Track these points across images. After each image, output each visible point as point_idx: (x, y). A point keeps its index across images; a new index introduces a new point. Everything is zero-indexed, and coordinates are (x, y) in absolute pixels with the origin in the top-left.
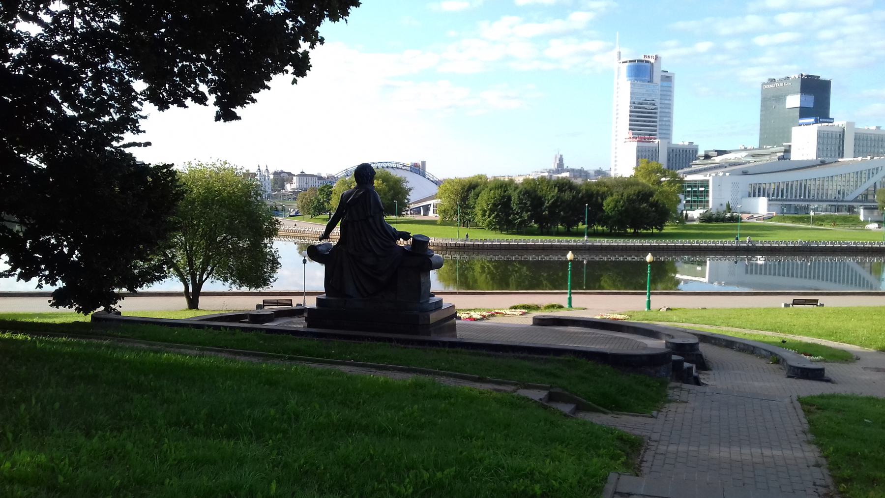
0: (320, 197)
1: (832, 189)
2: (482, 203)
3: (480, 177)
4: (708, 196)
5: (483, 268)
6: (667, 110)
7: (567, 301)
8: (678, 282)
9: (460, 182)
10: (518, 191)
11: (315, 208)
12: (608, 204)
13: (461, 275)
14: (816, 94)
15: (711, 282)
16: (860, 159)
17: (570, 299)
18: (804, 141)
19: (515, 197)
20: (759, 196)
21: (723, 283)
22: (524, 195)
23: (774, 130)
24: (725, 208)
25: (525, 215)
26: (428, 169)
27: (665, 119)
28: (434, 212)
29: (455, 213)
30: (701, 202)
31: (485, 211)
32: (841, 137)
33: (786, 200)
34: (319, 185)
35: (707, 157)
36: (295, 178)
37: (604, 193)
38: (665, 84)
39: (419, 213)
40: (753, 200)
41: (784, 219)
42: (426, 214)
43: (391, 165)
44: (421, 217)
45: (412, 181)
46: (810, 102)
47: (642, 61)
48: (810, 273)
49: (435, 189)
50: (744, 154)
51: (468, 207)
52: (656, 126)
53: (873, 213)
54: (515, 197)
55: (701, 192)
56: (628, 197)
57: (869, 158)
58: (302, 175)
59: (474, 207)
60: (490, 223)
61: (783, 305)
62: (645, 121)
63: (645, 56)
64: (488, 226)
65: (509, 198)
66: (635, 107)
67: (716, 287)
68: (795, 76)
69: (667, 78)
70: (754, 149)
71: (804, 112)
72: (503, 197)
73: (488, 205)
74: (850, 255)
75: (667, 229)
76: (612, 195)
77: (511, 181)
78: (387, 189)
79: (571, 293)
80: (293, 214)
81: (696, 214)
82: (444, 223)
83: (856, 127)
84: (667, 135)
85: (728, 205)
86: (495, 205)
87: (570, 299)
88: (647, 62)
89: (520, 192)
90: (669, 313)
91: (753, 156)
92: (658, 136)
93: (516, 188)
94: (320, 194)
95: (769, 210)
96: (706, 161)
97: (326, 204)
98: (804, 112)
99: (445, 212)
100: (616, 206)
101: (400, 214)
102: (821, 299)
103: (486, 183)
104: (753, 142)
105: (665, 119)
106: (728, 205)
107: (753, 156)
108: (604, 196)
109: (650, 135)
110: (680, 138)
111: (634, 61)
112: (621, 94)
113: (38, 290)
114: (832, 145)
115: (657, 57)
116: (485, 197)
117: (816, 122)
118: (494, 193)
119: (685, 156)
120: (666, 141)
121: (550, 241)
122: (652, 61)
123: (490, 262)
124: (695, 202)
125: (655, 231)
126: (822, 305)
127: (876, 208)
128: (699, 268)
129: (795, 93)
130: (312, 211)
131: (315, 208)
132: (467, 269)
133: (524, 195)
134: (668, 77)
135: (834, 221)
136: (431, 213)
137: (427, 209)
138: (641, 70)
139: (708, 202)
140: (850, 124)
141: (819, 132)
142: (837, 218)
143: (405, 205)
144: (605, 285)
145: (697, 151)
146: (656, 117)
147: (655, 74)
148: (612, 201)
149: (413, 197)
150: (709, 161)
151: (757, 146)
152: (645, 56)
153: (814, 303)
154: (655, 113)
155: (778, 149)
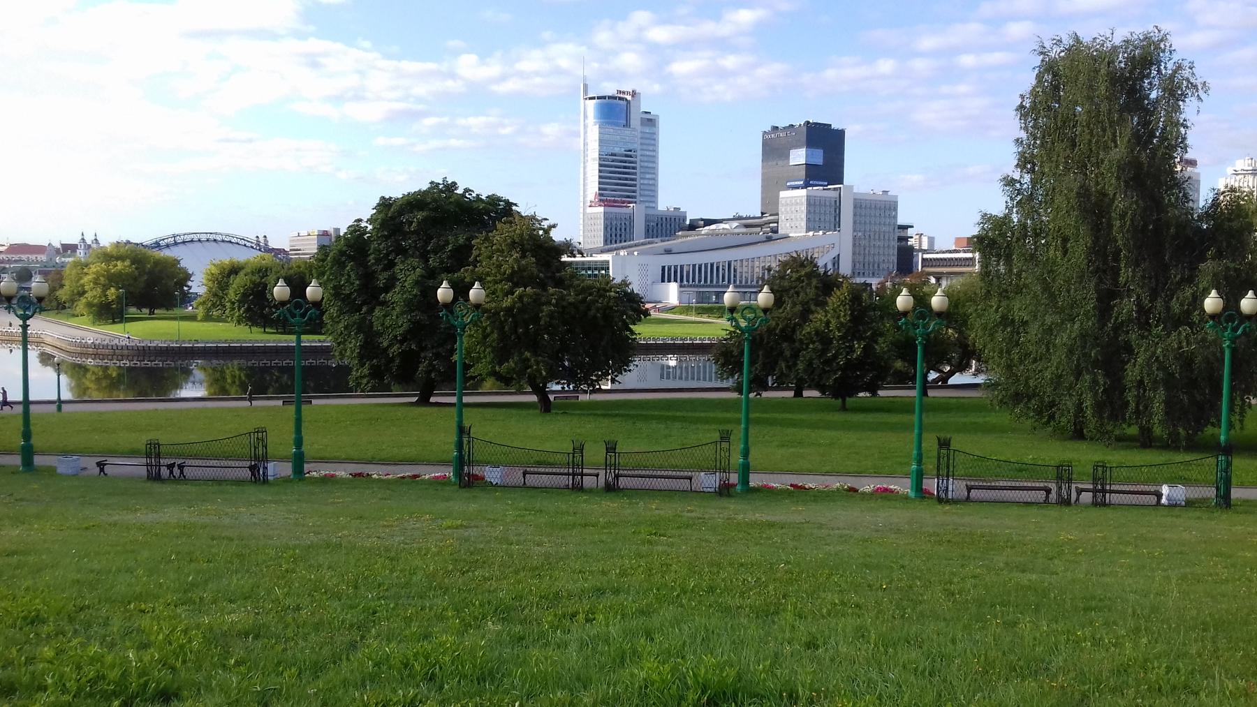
5: (233, 377)
14: (826, 145)
16: (811, 233)
20: (669, 281)
43: (212, 237)
46: (818, 158)
48: (705, 372)
50: (735, 224)
69: (650, 121)
78: (136, 273)
86: (245, 295)
88: (620, 99)
91: (747, 226)
107: (747, 226)
111: (604, 98)
112: (588, 138)
113: (729, 427)
121: (286, 341)
122: (629, 98)
129: (800, 147)
138: (615, 109)
147: (632, 116)
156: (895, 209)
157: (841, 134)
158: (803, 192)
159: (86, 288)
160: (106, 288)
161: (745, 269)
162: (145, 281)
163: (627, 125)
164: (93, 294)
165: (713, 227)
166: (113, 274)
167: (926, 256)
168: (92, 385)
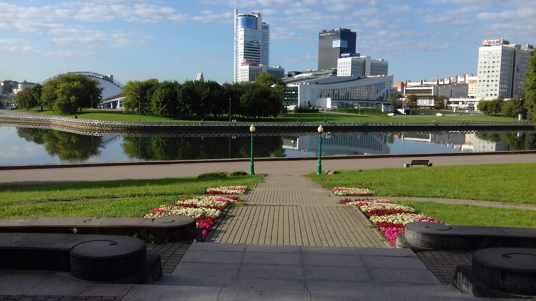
0: (34, 94)
1: (365, 95)
2: (156, 97)
3: (154, 81)
4: (297, 97)
5: (158, 143)
6: (266, 47)
7: (250, 168)
8: (284, 150)
9: (139, 84)
10: (182, 89)
11: (30, 102)
12: (243, 98)
13: (142, 149)
14: (349, 39)
15: (300, 150)
17: (253, 166)
18: (344, 66)
19: (180, 93)
21: (306, 150)
22: (186, 92)
23: (327, 61)
24: (307, 104)
25: (188, 106)
26: (115, 78)
27: (265, 52)
28: (121, 106)
29: (137, 105)
30: (293, 100)
31: (158, 103)
32: (363, 64)
33: (341, 100)
34: (32, 87)
35: (290, 75)
36: (19, 85)
37: (240, 92)
38: (264, 31)
39: (109, 107)
40: (323, 100)
41: (341, 111)
42: (115, 107)
43: (95, 75)
44: (111, 109)
45: (103, 84)
47: (251, 16)
49: (119, 91)
50: (311, 74)
51: (145, 100)
52: (259, 56)
53: (388, 107)
54: (180, 93)
55: (293, 94)
56: (256, 94)
57: (384, 75)
58: (25, 83)
59: (150, 101)
60: (162, 111)
61: (405, 166)
62: (253, 53)
63: (252, 13)
64: (161, 113)
65: (176, 94)
66: (248, 44)
67: (304, 154)
68: (337, 29)
70: (315, 71)
71: (343, 50)
72: (172, 93)
73: (161, 99)
74: (373, 131)
75: (279, 117)
76: (245, 93)
77: (176, 83)
79: (254, 160)
80: (14, 107)
81: (291, 107)
82: (128, 113)
83: (372, 59)
84: (266, 62)
85: (309, 102)
86: (165, 99)
87: (253, 166)
88: (254, 16)
89: (184, 90)
90: (337, 177)
92: (261, 62)
93: (181, 87)
94: (34, 92)
95: (332, 105)
96: (289, 78)
97: (38, 99)
98: (343, 50)
99: (128, 105)
100: (248, 100)
101: (95, 107)
102: (431, 160)
103: (158, 84)
104: (315, 68)
105: (265, 52)
106: (309, 102)
108: (240, 93)
109: (256, 61)
110: (274, 64)
111: (246, 16)
114: (359, 68)
115: (259, 14)
116: (159, 94)
117: (351, 56)
118: (165, 91)
119: (277, 75)
120: (266, 65)
122: (257, 16)
123: (163, 139)
124: (289, 100)
125: (272, 117)
126: (431, 165)
127: (390, 105)
128: (293, 141)
129: (336, 39)
130: (28, 105)
131: (30, 102)
132: (146, 144)
133: (186, 92)
134: (266, 27)
135: (369, 111)
136: (118, 107)
137: (115, 104)
139: (297, 100)
140: (369, 57)
141: (352, 61)
142: (370, 110)
143: (99, 101)
144: (243, 154)
145: (283, 72)
146: (259, 51)
148: (246, 97)
149: (105, 95)
150: (291, 78)
151: (317, 70)
152: (252, 13)
153: (425, 163)
154: (259, 48)
155: (329, 71)
156: (387, 68)
157: (354, 34)
158: (350, 58)
159: (58, 95)
160: (69, 96)
161: (343, 94)
162: (82, 93)
163: (256, 28)
164: (61, 99)
165: (300, 75)
166: (73, 88)
167: (407, 88)
168: (61, 147)
